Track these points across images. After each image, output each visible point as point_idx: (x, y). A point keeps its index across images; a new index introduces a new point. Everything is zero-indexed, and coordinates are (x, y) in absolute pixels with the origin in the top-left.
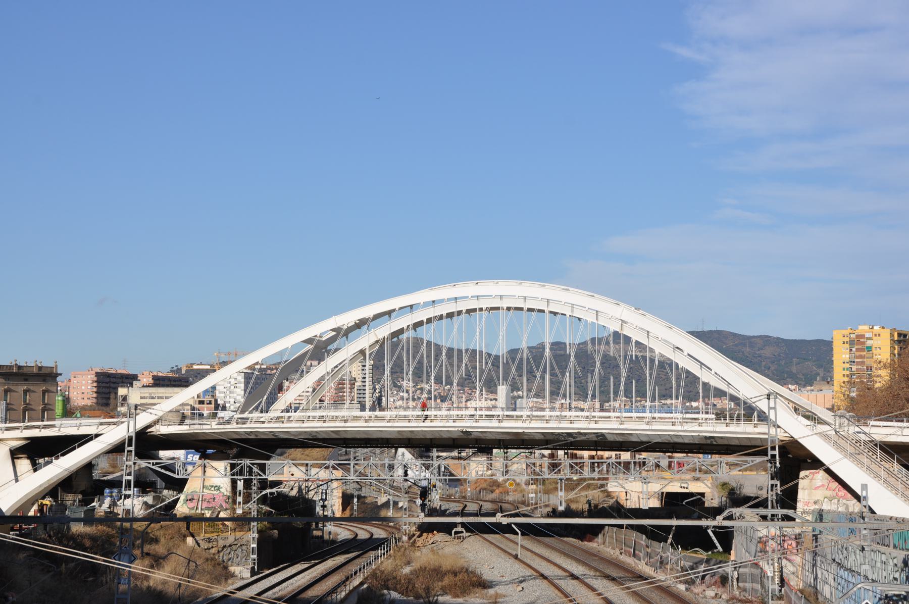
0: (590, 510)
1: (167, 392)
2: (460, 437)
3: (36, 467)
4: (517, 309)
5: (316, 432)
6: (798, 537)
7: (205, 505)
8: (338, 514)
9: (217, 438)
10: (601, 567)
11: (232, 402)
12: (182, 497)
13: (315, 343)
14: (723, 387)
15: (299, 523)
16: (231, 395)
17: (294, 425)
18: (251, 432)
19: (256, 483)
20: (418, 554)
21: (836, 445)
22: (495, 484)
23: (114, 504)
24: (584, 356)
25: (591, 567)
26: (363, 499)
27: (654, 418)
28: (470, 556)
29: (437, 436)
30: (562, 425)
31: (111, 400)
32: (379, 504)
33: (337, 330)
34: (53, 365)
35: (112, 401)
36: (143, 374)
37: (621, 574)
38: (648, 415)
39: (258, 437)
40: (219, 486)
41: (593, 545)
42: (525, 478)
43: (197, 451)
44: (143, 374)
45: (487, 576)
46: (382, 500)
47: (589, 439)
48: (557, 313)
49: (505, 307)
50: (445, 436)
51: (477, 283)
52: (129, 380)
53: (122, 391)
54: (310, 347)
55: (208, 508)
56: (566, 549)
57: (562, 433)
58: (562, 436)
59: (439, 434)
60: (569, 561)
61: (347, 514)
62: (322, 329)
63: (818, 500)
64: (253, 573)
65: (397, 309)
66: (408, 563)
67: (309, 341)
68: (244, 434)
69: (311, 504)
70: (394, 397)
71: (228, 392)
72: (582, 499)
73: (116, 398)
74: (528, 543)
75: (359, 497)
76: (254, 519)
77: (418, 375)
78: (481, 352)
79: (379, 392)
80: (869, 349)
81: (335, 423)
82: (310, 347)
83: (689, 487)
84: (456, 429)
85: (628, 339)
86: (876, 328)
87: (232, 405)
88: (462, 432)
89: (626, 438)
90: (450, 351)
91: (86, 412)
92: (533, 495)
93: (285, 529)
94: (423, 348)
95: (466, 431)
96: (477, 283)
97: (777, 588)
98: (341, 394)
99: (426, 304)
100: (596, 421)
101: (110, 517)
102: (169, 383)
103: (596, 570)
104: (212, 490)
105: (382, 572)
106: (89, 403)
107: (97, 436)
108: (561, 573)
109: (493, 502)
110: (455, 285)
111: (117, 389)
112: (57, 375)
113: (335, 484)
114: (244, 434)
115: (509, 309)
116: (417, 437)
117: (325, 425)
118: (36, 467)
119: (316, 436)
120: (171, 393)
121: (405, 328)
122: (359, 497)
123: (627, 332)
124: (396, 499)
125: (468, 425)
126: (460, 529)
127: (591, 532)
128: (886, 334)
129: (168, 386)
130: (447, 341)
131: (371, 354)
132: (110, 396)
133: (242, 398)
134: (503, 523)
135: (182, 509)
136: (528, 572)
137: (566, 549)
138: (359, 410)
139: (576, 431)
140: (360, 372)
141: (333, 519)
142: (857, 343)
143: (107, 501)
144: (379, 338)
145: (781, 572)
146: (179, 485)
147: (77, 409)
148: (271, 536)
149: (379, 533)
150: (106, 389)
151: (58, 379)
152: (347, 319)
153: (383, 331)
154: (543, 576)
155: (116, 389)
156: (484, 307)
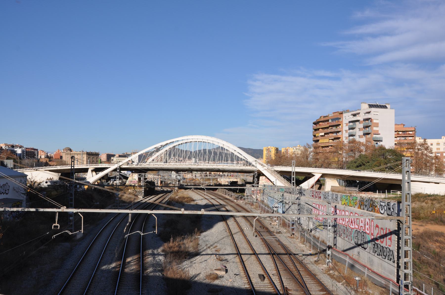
0: (215, 185)
3: (97, 174)
4: (196, 141)
6: (260, 190)
7: (133, 183)
8: (160, 185)
10: (218, 197)
12: (128, 181)
14: (245, 159)
15: (152, 187)
17: (152, 166)
20: (179, 194)
21: (268, 171)
22: (193, 179)
23: (113, 182)
24: (210, 152)
25: (216, 197)
28: (190, 194)
29: (183, 169)
30: (210, 167)
32: (168, 183)
33: (162, 146)
34: (98, 152)
35: (110, 160)
37: (223, 198)
38: (229, 165)
41: (216, 192)
42: (200, 178)
43: (131, 171)
45: (194, 199)
46: (169, 182)
49: (198, 141)
50: (185, 169)
52: (114, 156)
53: (112, 158)
54: (155, 149)
55: (133, 184)
56: (211, 193)
60: (211, 196)
61: (161, 185)
62: (158, 145)
64: (143, 198)
66: (177, 196)
67: (155, 148)
69: (154, 183)
72: (212, 183)
73: (111, 159)
74: (208, 191)
75: (164, 182)
76: (143, 186)
77: (174, 155)
78: (188, 151)
80: (270, 151)
82: (155, 149)
85: (225, 149)
86: (272, 147)
90: (181, 150)
91: (105, 162)
92: (202, 182)
93: (150, 188)
94: (180, 150)
97: (256, 201)
99: (181, 140)
101: (112, 185)
103: (217, 197)
105: (172, 197)
106: (105, 160)
107: (110, 168)
108: (210, 198)
109: (193, 183)
112: (99, 154)
113: (159, 179)
118: (97, 174)
122: (164, 182)
123: (224, 147)
124: (172, 182)
125: (190, 166)
126: (193, 189)
127: (216, 189)
128: (274, 148)
129: (122, 157)
130: (185, 149)
131: (169, 151)
135: (127, 183)
136: (203, 198)
137: (211, 193)
141: (159, 186)
142: (268, 150)
143: (112, 181)
145: (257, 197)
146: (127, 178)
148: (147, 190)
149: (169, 189)
151: (99, 155)
152: (164, 143)
153: (171, 146)
154: (206, 199)
155: (111, 158)
156: (189, 142)
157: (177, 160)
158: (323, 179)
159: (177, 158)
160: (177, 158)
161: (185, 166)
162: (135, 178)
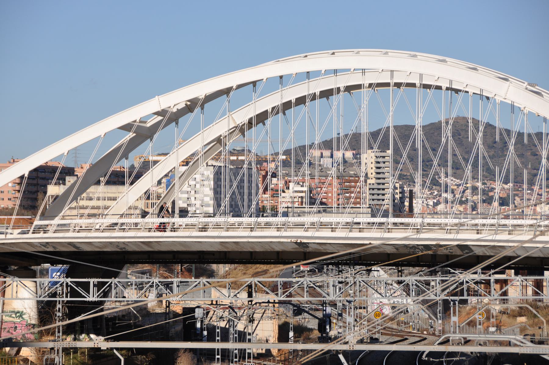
1: (109, 191)
2: (295, 250)
5: (124, 243)
9: (8, 251)
11: (198, 206)
13: (134, 129)
16: (197, 196)
18: (47, 243)
19: (61, 307)
26: (308, 333)
27: (259, 224)
29: (268, 249)
30: (352, 235)
31: (39, 202)
36: (82, 168)
39: (57, 250)
40: (22, 312)
44: (82, 168)
47: (452, 253)
48: (460, 91)
49: (366, 83)
51: (333, 54)
57: (417, 245)
58: (418, 249)
59: (270, 246)
65: (234, 87)
67: (127, 128)
68: (39, 245)
70: (434, 198)
71: (193, 192)
79: (400, 193)
81: (370, 232)
84: (289, 240)
88: (296, 243)
95: (301, 243)
96: (333, 54)
98: (348, 195)
100: (478, 230)
102: (116, 179)
104: (14, 318)
110: (306, 56)
114: (39, 245)
115: (370, 85)
116: (245, 250)
117: (254, 234)
119: (124, 248)
120: (115, 193)
121: (270, 111)
132: (37, 196)
133: (211, 200)
134: (102, 349)
138: (370, 215)
139: (434, 243)
140: (373, 166)
144: (238, 123)
147: (407, 215)
150: (33, 187)
155: (45, 186)
157: (478, 198)
158: (77, 330)
159: (479, 185)
160: (479, 185)
161: (187, 234)
162: (17, 305)
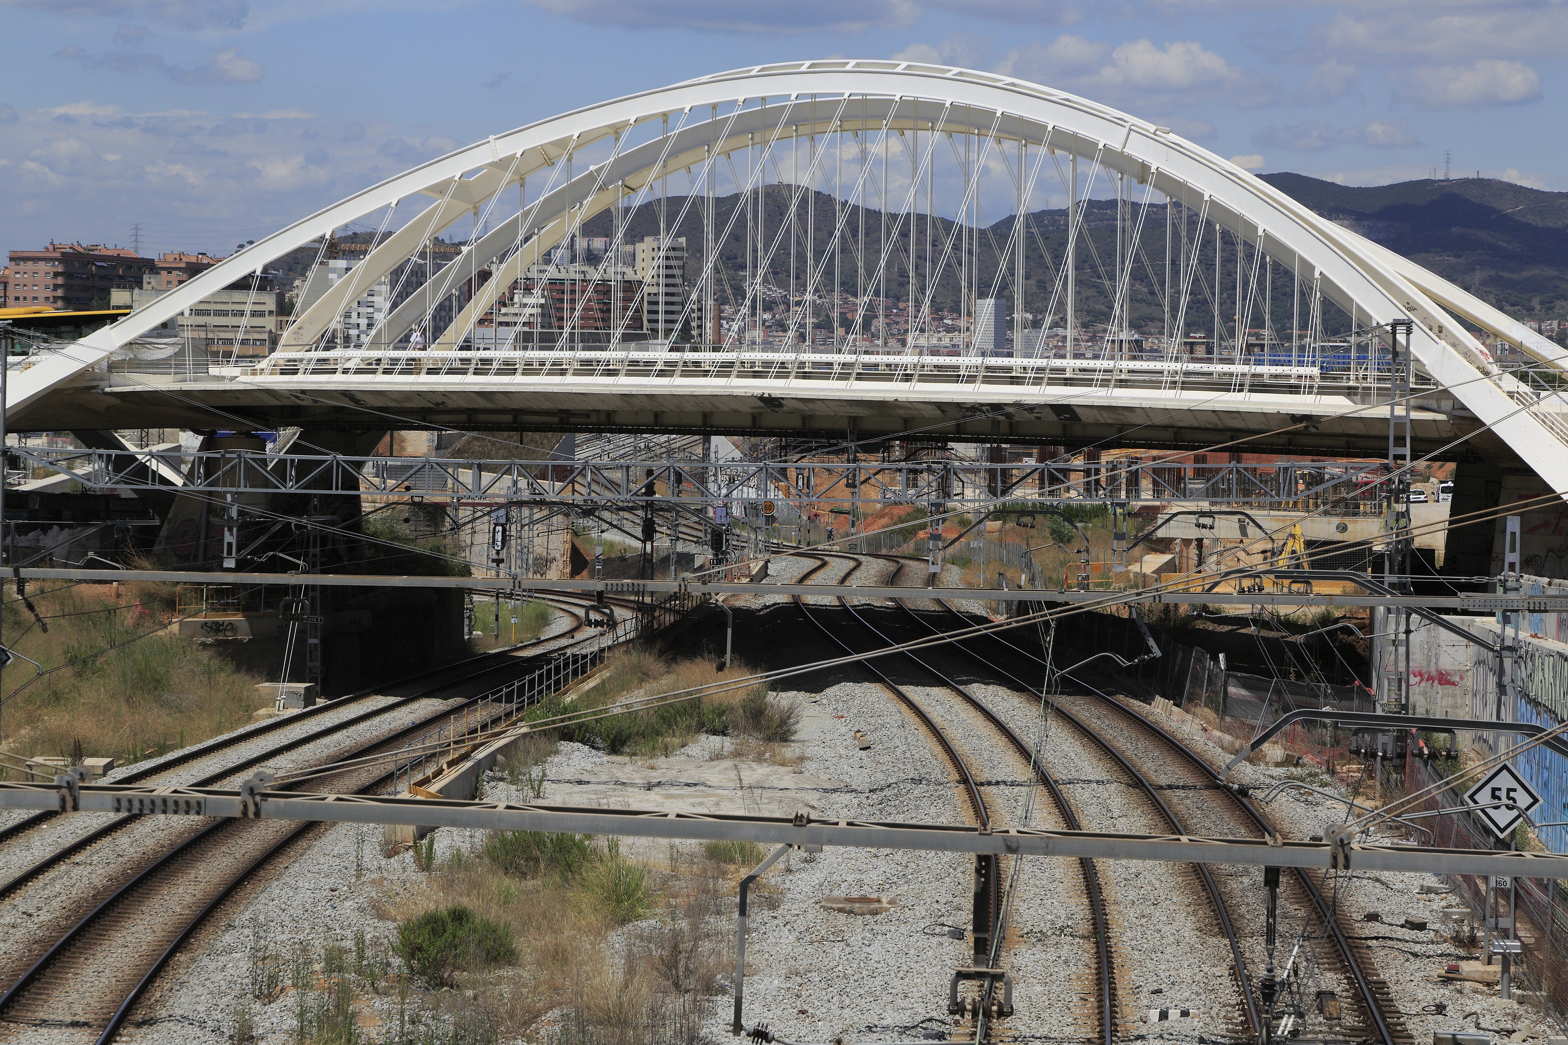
58: (981, 411)
63: (1534, 556)
83: (1216, 525)
87: (363, 332)
89: (1120, 417)
111: (109, 293)
